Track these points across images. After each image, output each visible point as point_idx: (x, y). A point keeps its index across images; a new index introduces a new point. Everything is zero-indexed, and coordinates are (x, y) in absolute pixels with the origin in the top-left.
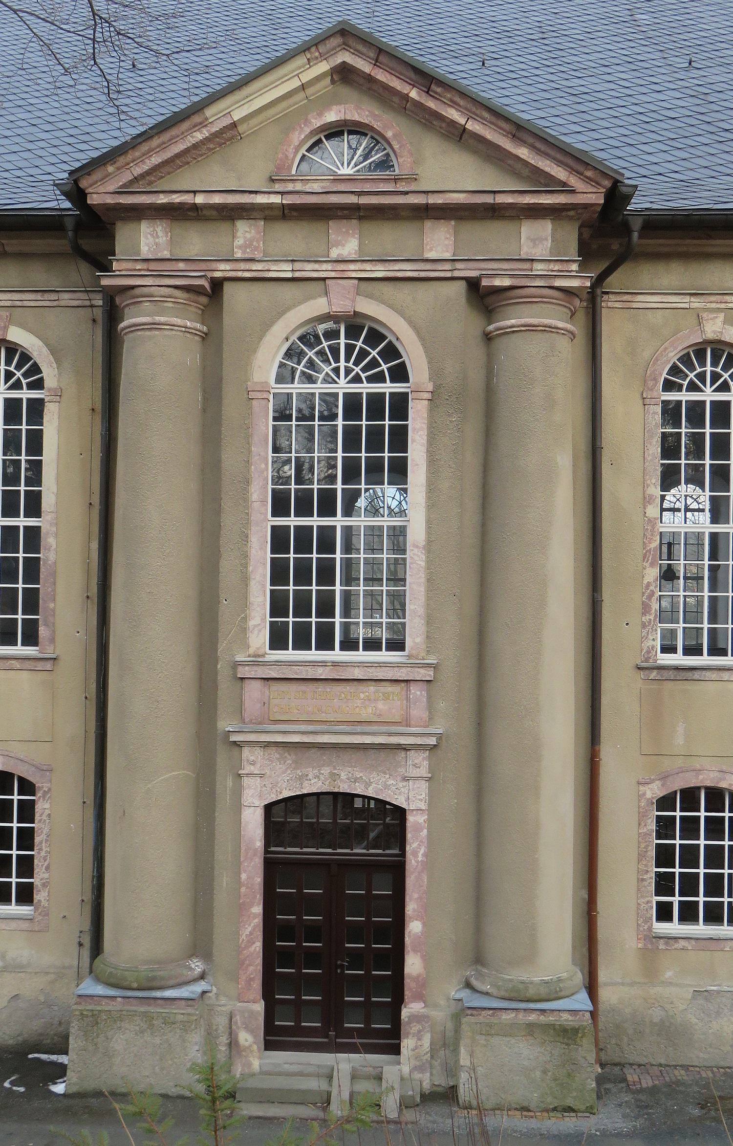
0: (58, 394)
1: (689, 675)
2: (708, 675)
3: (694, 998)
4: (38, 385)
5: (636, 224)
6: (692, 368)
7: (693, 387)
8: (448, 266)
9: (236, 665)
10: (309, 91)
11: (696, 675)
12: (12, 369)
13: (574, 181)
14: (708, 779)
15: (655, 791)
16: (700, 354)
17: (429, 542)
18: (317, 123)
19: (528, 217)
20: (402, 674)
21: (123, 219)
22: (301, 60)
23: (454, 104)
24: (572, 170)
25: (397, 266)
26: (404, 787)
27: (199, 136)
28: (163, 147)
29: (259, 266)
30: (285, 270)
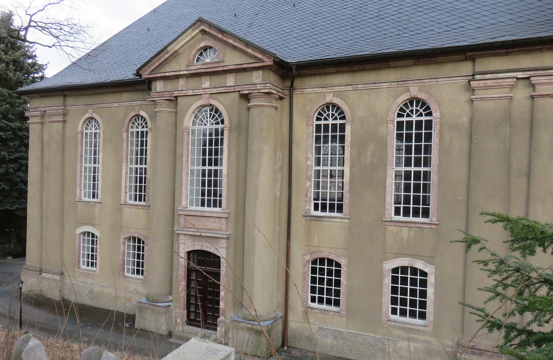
0: (151, 129)
1: (319, 219)
2: (326, 219)
3: (318, 330)
4: (343, 118)
5: (294, 67)
6: (408, 108)
7: (408, 115)
8: (233, 88)
9: (178, 210)
10: (196, 38)
11: (322, 219)
12: (418, 108)
13: (264, 58)
14: (325, 255)
15: (308, 258)
16: (411, 103)
17: (228, 174)
18: (198, 47)
19: (255, 70)
20: (219, 215)
21: (153, 81)
22: (190, 30)
23: (230, 38)
24: (263, 55)
25: (219, 89)
26: (220, 250)
27: (167, 56)
28: (158, 60)
29: (184, 92)
30: (190, 92)
